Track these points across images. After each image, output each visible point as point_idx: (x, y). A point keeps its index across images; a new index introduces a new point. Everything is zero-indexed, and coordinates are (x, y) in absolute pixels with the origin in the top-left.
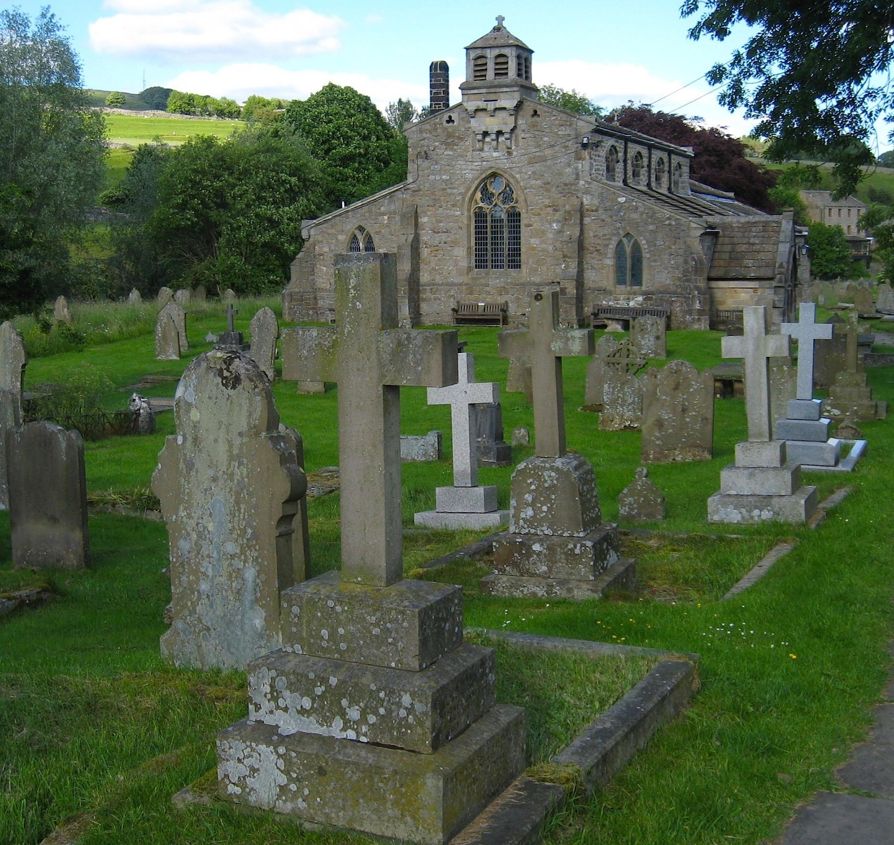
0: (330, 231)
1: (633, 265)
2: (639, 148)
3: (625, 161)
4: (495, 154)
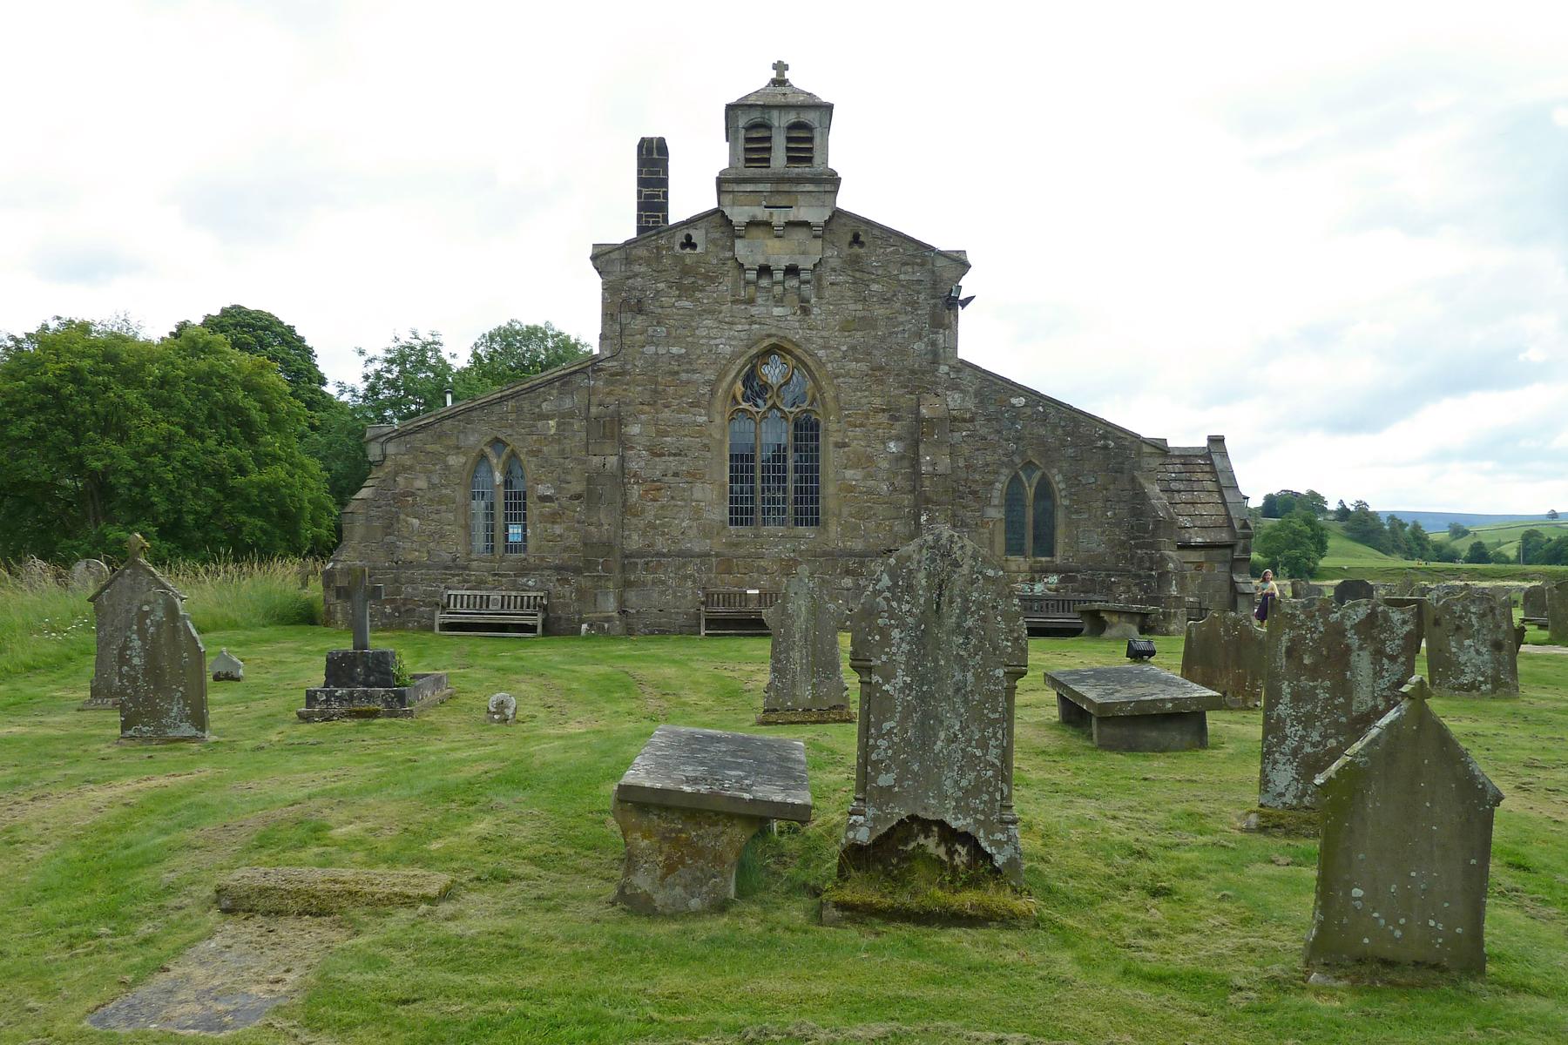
0: (429, 448)
4: (777, 311)
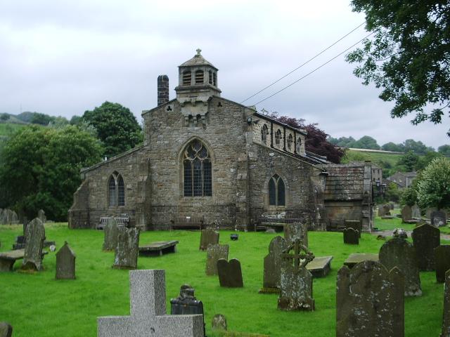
1: (279, 193)
2: (279, 127)
3: (272, 134)
4: (196, 128)
